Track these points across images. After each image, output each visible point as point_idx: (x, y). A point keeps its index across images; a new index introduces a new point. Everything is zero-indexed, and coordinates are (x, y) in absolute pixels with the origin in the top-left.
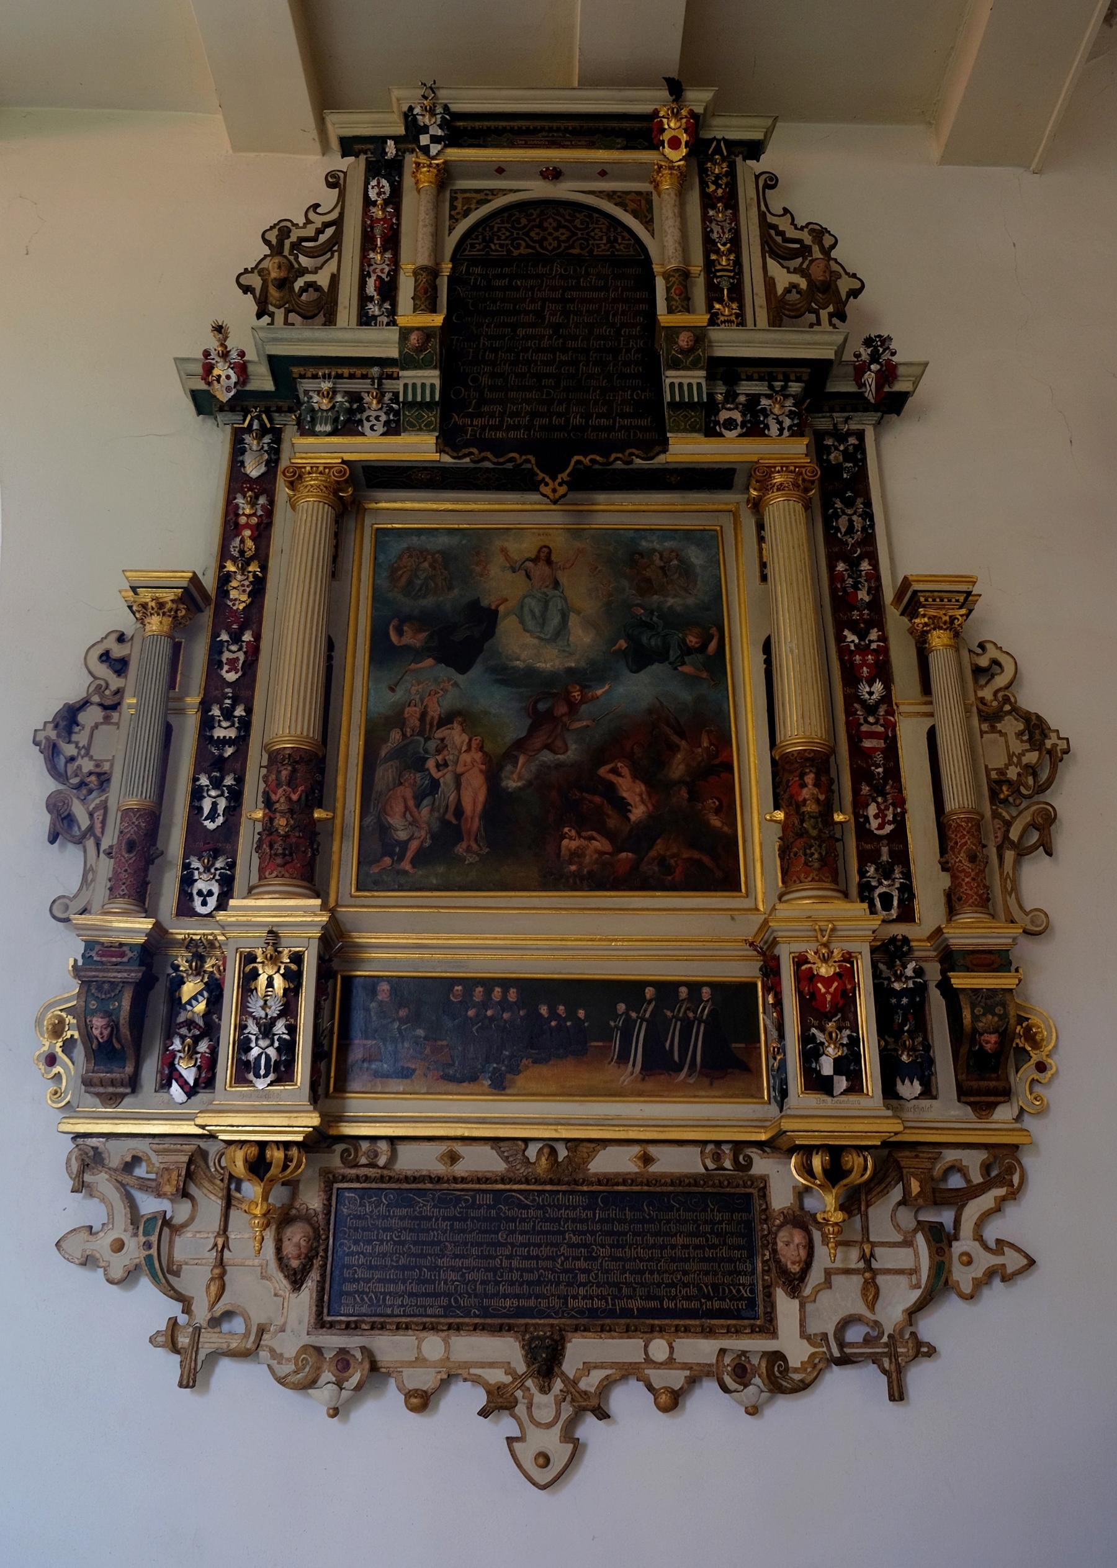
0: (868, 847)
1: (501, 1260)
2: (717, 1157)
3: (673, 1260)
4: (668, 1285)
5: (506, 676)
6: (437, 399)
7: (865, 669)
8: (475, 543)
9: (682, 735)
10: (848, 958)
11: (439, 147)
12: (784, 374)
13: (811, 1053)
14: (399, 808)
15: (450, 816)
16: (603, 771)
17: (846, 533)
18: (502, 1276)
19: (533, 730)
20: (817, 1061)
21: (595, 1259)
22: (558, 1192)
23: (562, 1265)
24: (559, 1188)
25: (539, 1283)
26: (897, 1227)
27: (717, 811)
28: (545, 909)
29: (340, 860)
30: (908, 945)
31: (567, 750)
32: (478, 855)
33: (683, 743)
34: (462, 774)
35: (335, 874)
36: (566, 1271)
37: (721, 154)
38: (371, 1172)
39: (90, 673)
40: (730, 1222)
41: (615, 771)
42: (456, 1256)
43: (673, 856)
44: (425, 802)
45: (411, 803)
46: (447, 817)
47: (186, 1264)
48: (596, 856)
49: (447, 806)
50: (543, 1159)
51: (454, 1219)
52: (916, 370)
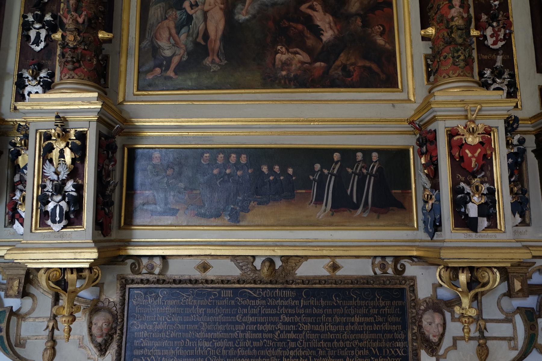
0: (485, 57)
1: (238, 333)
2: (383, 267)
3: (352, 332)
4: (349, 349)
10: (488, 131)
13: (460, 201)
14: (165, 35)
15: (200, 40)
16: (304, 8)
18: (239, 344)
20: (466, 208)
21: (301, 332)
22: (276, 288)
23: (279, 336)
24: (276, 286)
25: (263, 348)
26: (501, 309)
27: (382, 34)
28: (265, 101)
29: (126, 70)
30: (518, 123)
32: (220, 65)
34: (208, 11)
35: (122, 80)
36: (281, 340)
38: (151, 277)
40: (390, 307)
41: (312, 8)
42: (208, 331)
43: (352, 64)
44: (183, 30)
45: (174, 31)
46: (198, 40)
47: (29, 339)
48: (299, 65)
49: (198, 33)
50: (265, 269)
51: (207, 306)
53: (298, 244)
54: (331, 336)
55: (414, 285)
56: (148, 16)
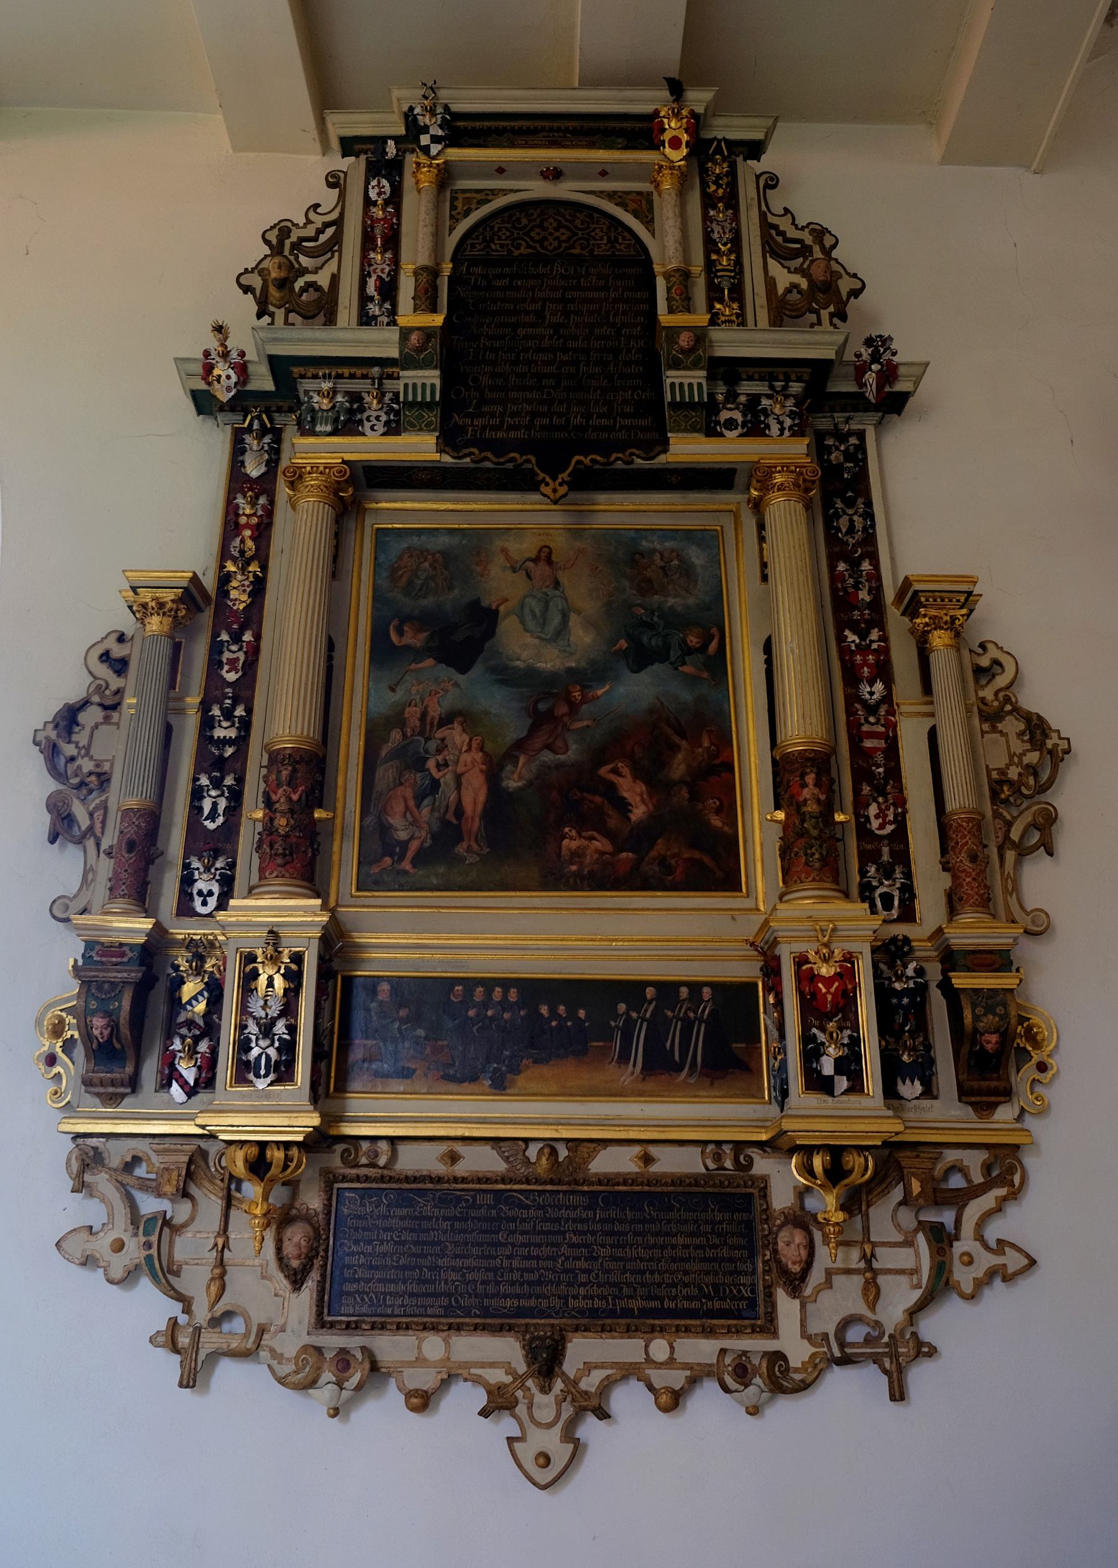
0: (869, 847)
1: (502, 1260)
2: (718, 1157)
3: (674, 1260)
4: (669, 1285)
5: (506, 676)
6: (437, 399)
7: (866, 669)
8: (475, 543)
9: (683, 735)
10: (849, 958)
11: (440, 147)
12: (785, 374)
13: (811, 1053)
14: (399, 808)
15: (450, 816)
16: (603, 771)
17: (847, 533)
18: (502, 1276)
19: (533, 730)
20: (818, 1061)
21: (596, 1259)
22: (558, 1192)
23: (563, 1265)
24: (559, 1188)
25: (539, 1283)
26: (898, 1227)
27: (718, 811)
28: (545, 909)
30: (909, 945)
31: (567, 750)
32: (479, 855)
33: (684, 742)
34: (463, 774)
35: (335, 874)
36: (566, 1271)
37: (722, 154)
38: (371, 1172)
39: (90, 673)
41: (615, 771)
42: (456, 1256)
43: (673, 856)
44: (426, 802)
45: (411, 803)
47: (187, 1264)
48: (596, 856)
50: (544, 1159)
52: (916, 370)
53: (592, 1122)
54: (642, 1266)
55: (766, 1187)
56: (373, 781)
